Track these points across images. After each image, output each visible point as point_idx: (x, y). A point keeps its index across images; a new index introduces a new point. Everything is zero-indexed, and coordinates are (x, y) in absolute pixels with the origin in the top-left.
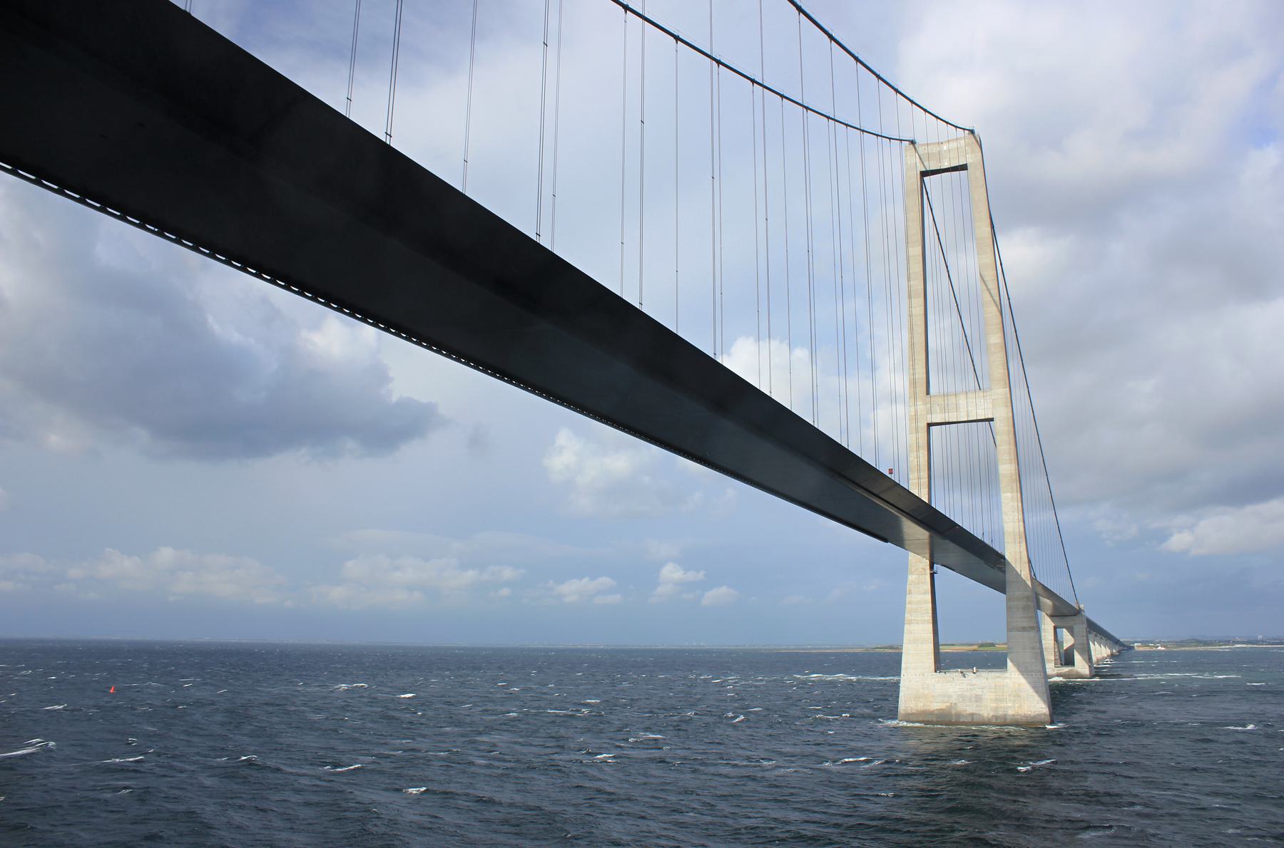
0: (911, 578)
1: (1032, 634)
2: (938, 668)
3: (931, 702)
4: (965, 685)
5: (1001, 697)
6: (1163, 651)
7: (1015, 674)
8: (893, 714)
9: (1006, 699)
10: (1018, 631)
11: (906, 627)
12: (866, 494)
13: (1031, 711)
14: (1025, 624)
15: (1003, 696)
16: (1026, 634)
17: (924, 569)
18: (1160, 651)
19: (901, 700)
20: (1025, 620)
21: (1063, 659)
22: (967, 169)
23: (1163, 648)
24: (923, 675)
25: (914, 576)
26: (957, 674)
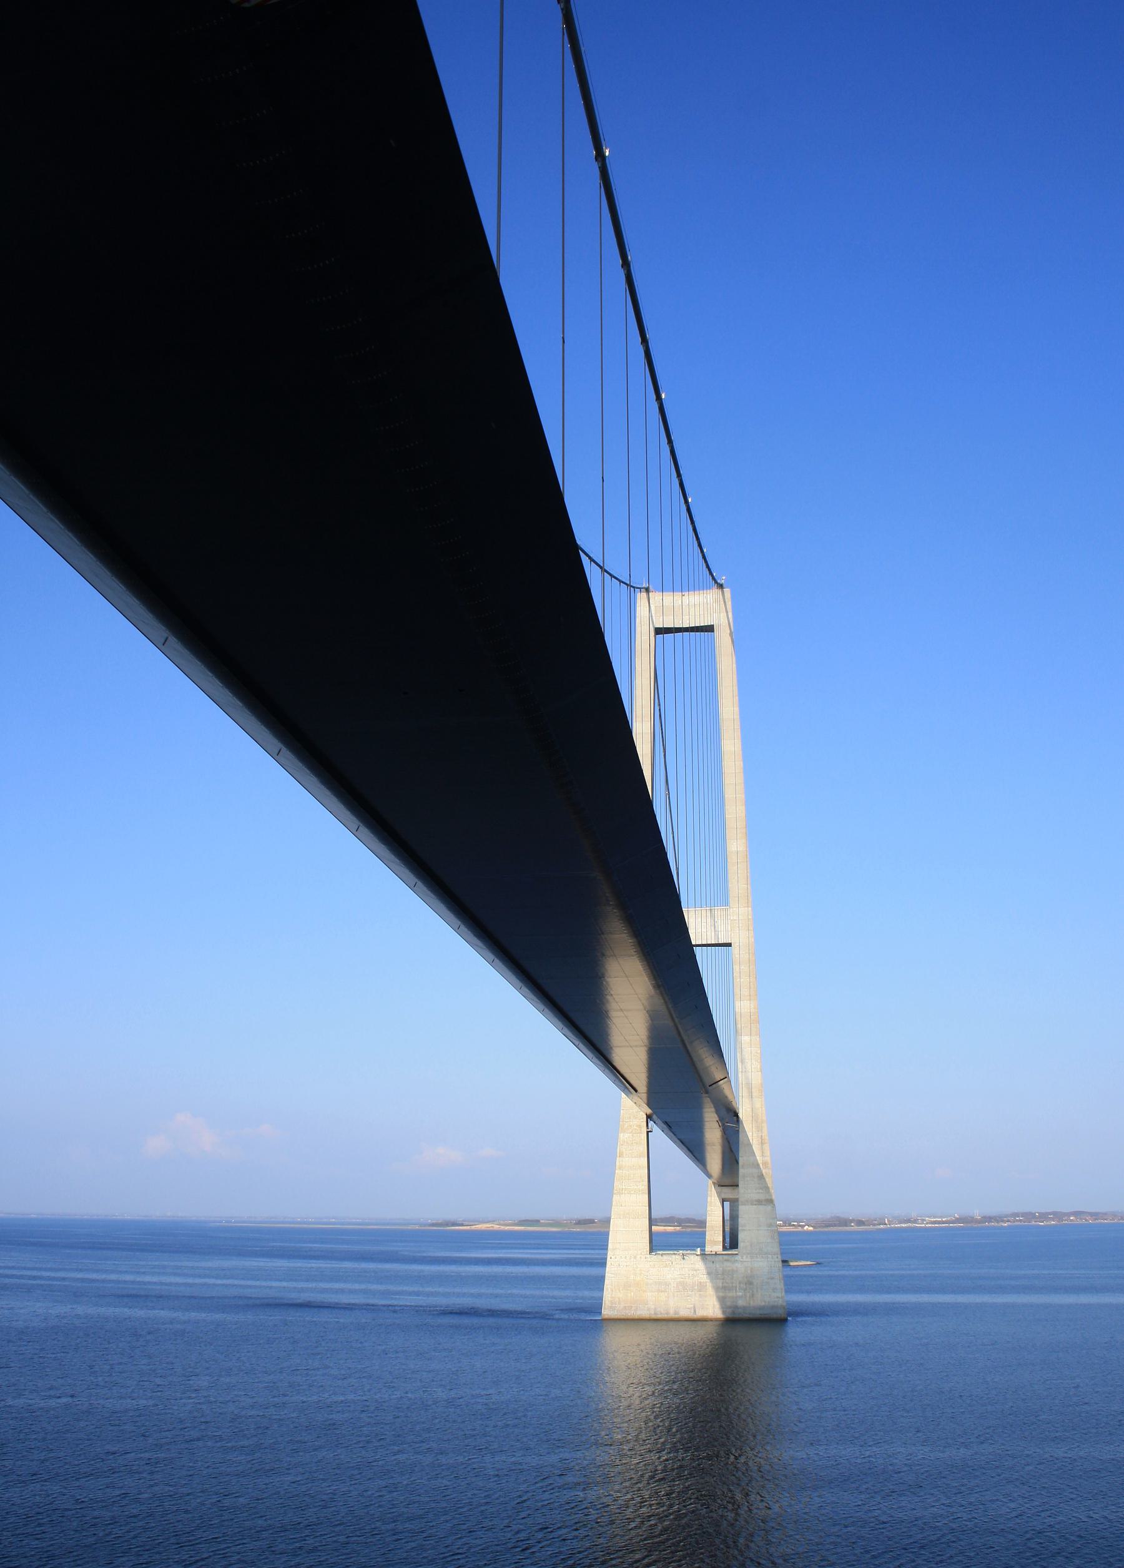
0: (623, 1137)
1: (769, 1208)
2: (652, 1249)
3: (644, 1291)
4: (687, 1269)
5: (731, 1285)
6: (811, 1231)
7: (747, 1257)
8: (600, 1313)
9: (736, 1287)
10: (752, 1205)
11: (615, 1198)
12: (583, 1316)
13: (765, 1302)
14: (756, 1197)
15: (732, 1283)
16: (761, 1208)
17: (640, 1126)
18: (808, 1232)
19: (607, 1289)
20: (761, 1191)
21: (728, 1240)
22: (713, 631)
23: (811, 1228)
24: (635, 1257)
25: (627, 1135)
26: (677, 1257)
